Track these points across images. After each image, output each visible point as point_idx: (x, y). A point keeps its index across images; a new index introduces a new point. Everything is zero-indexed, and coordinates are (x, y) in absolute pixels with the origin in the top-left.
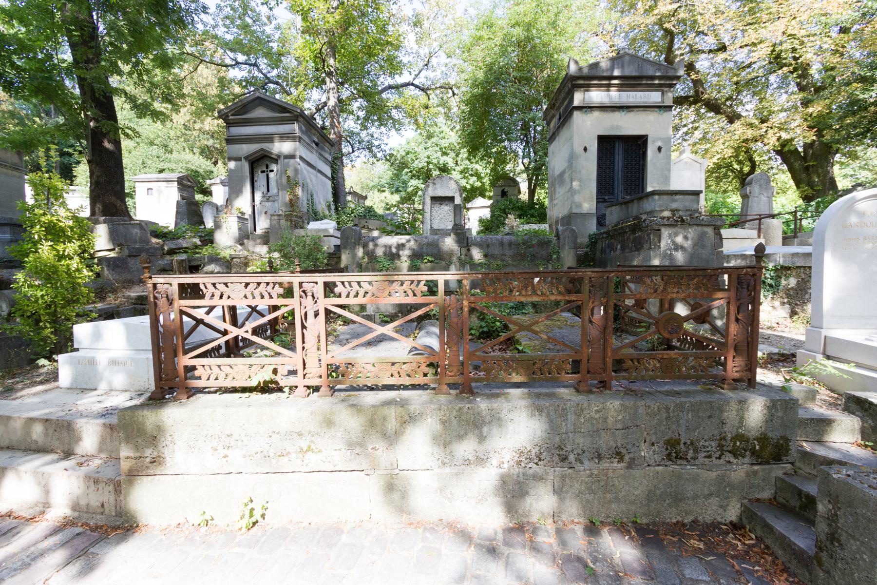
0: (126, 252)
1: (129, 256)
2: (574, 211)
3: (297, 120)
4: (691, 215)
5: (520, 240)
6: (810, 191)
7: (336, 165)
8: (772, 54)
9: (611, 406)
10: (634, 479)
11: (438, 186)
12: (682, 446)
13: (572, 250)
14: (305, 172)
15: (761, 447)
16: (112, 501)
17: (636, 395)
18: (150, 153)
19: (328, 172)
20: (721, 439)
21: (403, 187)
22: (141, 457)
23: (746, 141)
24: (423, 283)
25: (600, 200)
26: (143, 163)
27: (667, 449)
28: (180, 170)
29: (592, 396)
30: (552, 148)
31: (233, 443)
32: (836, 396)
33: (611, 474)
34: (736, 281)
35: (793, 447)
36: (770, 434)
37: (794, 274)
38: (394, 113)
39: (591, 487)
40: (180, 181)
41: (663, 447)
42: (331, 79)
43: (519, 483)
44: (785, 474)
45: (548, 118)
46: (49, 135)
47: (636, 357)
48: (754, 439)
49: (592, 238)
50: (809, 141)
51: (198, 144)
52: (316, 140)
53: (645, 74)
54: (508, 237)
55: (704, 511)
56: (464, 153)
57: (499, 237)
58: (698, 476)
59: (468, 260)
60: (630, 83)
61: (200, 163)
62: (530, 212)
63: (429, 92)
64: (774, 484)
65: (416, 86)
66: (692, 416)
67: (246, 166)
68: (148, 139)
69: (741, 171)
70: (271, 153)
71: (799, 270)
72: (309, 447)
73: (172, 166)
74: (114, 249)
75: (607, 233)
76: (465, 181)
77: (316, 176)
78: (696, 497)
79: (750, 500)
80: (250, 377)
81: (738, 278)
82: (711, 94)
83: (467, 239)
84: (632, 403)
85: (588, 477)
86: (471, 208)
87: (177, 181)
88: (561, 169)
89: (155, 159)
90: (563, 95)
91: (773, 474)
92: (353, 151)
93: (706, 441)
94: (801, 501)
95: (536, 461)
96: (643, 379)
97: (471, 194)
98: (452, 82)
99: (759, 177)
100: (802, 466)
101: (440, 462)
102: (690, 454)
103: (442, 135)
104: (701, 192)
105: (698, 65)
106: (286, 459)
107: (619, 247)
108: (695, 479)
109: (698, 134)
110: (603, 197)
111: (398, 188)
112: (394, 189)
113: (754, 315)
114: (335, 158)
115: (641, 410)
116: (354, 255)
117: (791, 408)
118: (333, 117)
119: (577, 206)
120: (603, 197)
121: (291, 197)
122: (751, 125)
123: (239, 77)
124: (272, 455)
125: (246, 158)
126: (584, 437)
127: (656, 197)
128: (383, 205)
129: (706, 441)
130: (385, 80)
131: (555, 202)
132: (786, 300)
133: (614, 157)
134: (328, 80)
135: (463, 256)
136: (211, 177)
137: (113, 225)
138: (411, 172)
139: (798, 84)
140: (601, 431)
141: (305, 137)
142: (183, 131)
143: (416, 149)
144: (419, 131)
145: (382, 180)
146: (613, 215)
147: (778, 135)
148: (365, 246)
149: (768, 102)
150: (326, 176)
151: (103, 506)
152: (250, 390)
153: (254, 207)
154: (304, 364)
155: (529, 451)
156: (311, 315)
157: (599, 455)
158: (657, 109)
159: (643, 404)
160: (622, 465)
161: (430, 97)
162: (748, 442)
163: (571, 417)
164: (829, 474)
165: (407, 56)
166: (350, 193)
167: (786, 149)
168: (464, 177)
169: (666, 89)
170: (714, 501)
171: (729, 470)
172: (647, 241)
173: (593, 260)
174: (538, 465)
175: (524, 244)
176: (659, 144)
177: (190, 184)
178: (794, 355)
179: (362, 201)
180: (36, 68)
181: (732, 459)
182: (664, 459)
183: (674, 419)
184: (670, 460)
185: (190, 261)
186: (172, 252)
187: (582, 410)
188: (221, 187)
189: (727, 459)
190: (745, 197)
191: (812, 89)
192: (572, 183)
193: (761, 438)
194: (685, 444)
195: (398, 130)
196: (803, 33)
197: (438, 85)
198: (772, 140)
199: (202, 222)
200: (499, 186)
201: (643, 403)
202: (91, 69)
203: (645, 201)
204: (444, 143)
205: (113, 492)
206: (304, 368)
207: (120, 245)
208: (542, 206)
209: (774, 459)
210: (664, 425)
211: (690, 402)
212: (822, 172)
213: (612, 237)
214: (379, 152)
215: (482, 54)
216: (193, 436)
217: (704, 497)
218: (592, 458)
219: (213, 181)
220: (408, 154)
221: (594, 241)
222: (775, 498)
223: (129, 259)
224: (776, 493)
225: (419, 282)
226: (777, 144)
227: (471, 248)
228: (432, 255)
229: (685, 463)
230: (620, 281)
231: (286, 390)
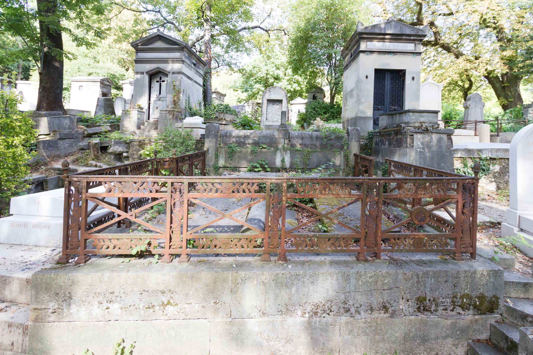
0: (58, 136)
1: (60, 139)
2: (359, 115)
4: (433, 126)
5: (323, 135)
6: (506, 102)
7: (207, 77)
8: (481, 19)
9: (380, 273)
10: (395, 325)
11: (272, 93)
12: (428, 301)
13: (357, 143)
15: (480, 303)
16: (20, 341)
17: (397, 264)
18: (84, 62)
19: (201, 81)
20: (453, 297)
22: (45, 309)
23: (466, 70)
24: (256, 184)
25: (375, 109)
27: (417, 304)
28: (103, 74)
29: (367, 265)
30: (345, 74)
31: (114, 299)
32: (528, 258)
33: (379, 322)
34: (462, 188)
35: (501, 303)
36: (486, 294)
37: (498, 163)
38: (247, 44)
39: (366, 331)
40: (102, 82)
41: (415, 303)
42: (207, 23)
44: (496, 322)
46: (15, 56)
47: (397, 237)
48: (476, 297)
49: (370, 135)
50: (504, 72)
51: (117, 57)
52: (194, 62)
53: (404, 33)
55: (442, 348)
56: (290, 71)
58: (438, 323)
60: (397, 38)
61: (118, 70)
62: (331, 110)
63: (269, 32)
64: (489, 329)
65: (262, 28)
66: (434, 281)
67: (147, 78)
68: (83, 53)
69: (463, 87)
71: (501, 161)
72: (169, 301)
73: (98, 71)
74: (50, 134)
75: (380, 132)
76: (290, 86)
78: (437, 338)
79: (473, 341)
80: (131, 247)
81: (463, 186)
82: (445, 39)
83: (289, 133)
84: (394, 271)
85: (364, 323)
87: (101, 82)
89: (87, 66)
90: (353, 43)
91: (489, 322)
92: (219, 67)
93: (443, 298)
94: (508, 344)
95: (328, 312)
96: (401, 251)
97: (293, 95)
98: (285, 26)
99: (475, 96)
100: (508, 317)
101: (261, 313)
102: (433, 308)
103: (277, 57)
104: (439, 111)
105: (436, 23)
106: (152, 310)
107: (387, 143)
108: (436, 325)
109: (436, 64)
110: (378, 107)
111: (246, 89)
112: (244, 90)
113: (474, 210)
114: (206, 73)
115: (400, 277)
117: (499, 276)
119: (361, 112)
120: (378, 107)
122: (470, 61)
123: (148, 19)
124: (141, 307)
125: (147, 73)
126: (361, 295)
127: (411, 114)
128: (237, 98)
129: (443, 298)
130: (241, 24)
131: (347, 108)
132: (493, 180)
134: (205, 24)
135: (285, 145)
136: (123, 78)
137: (51, 118)
138: (255, 79)
139: (497, 37)
140: (373, 291)
141: (187, 61)
142: (108, 49)
143: (260, 65)
144: (262, 55)
145: (236, 84)
146: (384, 121)
147: (486, 67)
149: (479, 47)
150: (199, 85)
151: (12, 344)
152: (131, 256)
153: (149, 104)
154: (171, 239)
155: (324, 305)
156: (178, 204)
157: (372, 308)
158: (412, 54)
159: (402, 272)
160: (387, 315)
161: (270, 35)
162: (471, 299)
163: (353, 281)
164: (526, 335)
165: (257, 9)
166: (215, 92)
167: (491, 76)
168: (290, 84)
169: (417, 42)
170: (449, 341)
171: (459, 319)
172: (405, 142)
173: (370, 149)
174: (329, 315)
177: (108, 83)
178: (499, 224)
179: (223, 97)
180: (12, 13)
181: (461, 312)
182: (415, 311)
183: (422, 283)
184: (419, 312)
185: (101, 143)
186: (90, 136)
187: (360, 276)
188: (129, 85)
189: (458, 311)
190: (466, 108)
191: (506, 40)
193: (480, 297)
194: (429, 300)
195: (248, 55)
196: (499, 8)
197: (275, 28)
198: (483, 72)
199: (113, 113)
201: (402, 271)
202: (49, 16)
203: (404, 115)
204: (278, 62)
205: (21, 334)
206: (170, 241)
207: (54, 131)
208: (339, 106)
209: (489, 311)
210: (416, 287)
211: (433, 271)
212: (513, 90)
213: (383, 136)
214: (235, 67)
215: (303, 13)
216: (85, 294)
217: (443, 338)
218: (367, 310)
219: (124, 82)
220: (254, 68)
221: (371, 137)
222: (490, 339)
223: (59, 141)
224: (490, 335)
225: (253, 184)
226: (485, 72)
229: (430, 314)
230: (387, 170)
231: (157, 257)
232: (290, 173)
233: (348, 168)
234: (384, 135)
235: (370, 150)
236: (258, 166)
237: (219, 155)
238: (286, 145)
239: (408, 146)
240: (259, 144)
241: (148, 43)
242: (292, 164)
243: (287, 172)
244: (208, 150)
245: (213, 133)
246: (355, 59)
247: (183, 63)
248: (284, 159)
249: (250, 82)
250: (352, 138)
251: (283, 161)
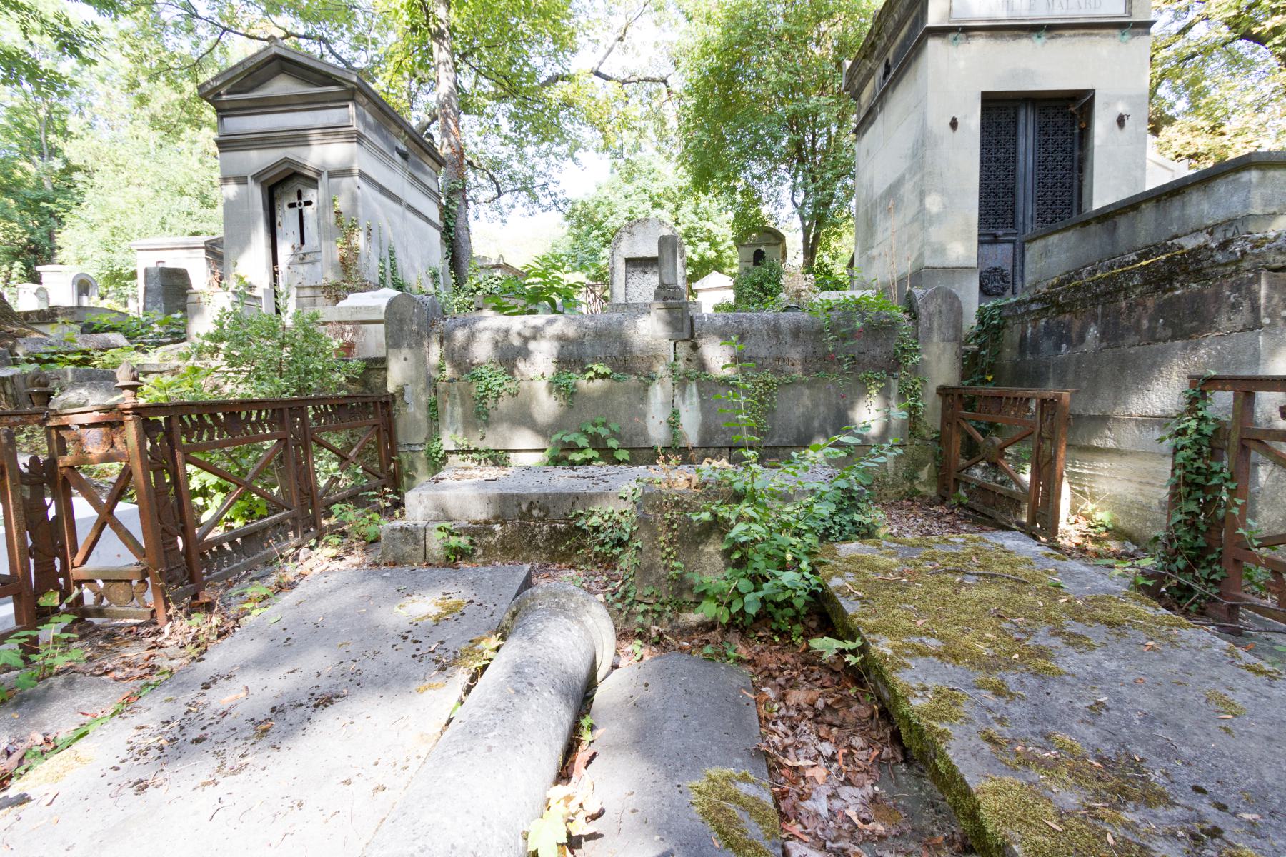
2: (929, 262)
3: (352, 99)
11: (638, 237)
13: (949, 346)
14: (376, 206)
25: (987, 238)
26: (163, 223)
42: (440, 44)
45: (857, 83)
52: (403, 148)
54: (790, 315)
57: (769, 314)
70: (304, 167)
76: (691, 248)
77: (404, 217)
87: (206, 248)
88: (892, 178)
110: (993, 231)
116: (422, 361)
118: (446, 116)
119: (934, 251)
120: (993, 231)
121: (344, 252)
125: (256, 178)
127: (1254, 175)
131: (875, 252)
133: (1015, 143)
134: (435, 46)
138: (603, 235)
143: (611, 198)
148: (445, 338)
150: (427, 220)
153: (275, 273)
158: (1116, 32)
175: (833, 331)
176: (1121, 108)
177: (811, 240)
192: (922, 201)
200: (750, 245)
204: (656, 188)
214: (545, 196)
227: (700, 342)
228: (604, 361)
232: (705, 465)
234: (1071, 303)
235: (990, 373)
236: (583, 442)
239: (1267, 321)
241: (249, 83)
242: (707, 433)
243: (686, 460)
244: (402, 391)
245: (414, 327)
246: (909, 66)
247: (359, 142)
248: (676, 413)
249: (591, 244)
250: (930, 329)
251: (673, 423)
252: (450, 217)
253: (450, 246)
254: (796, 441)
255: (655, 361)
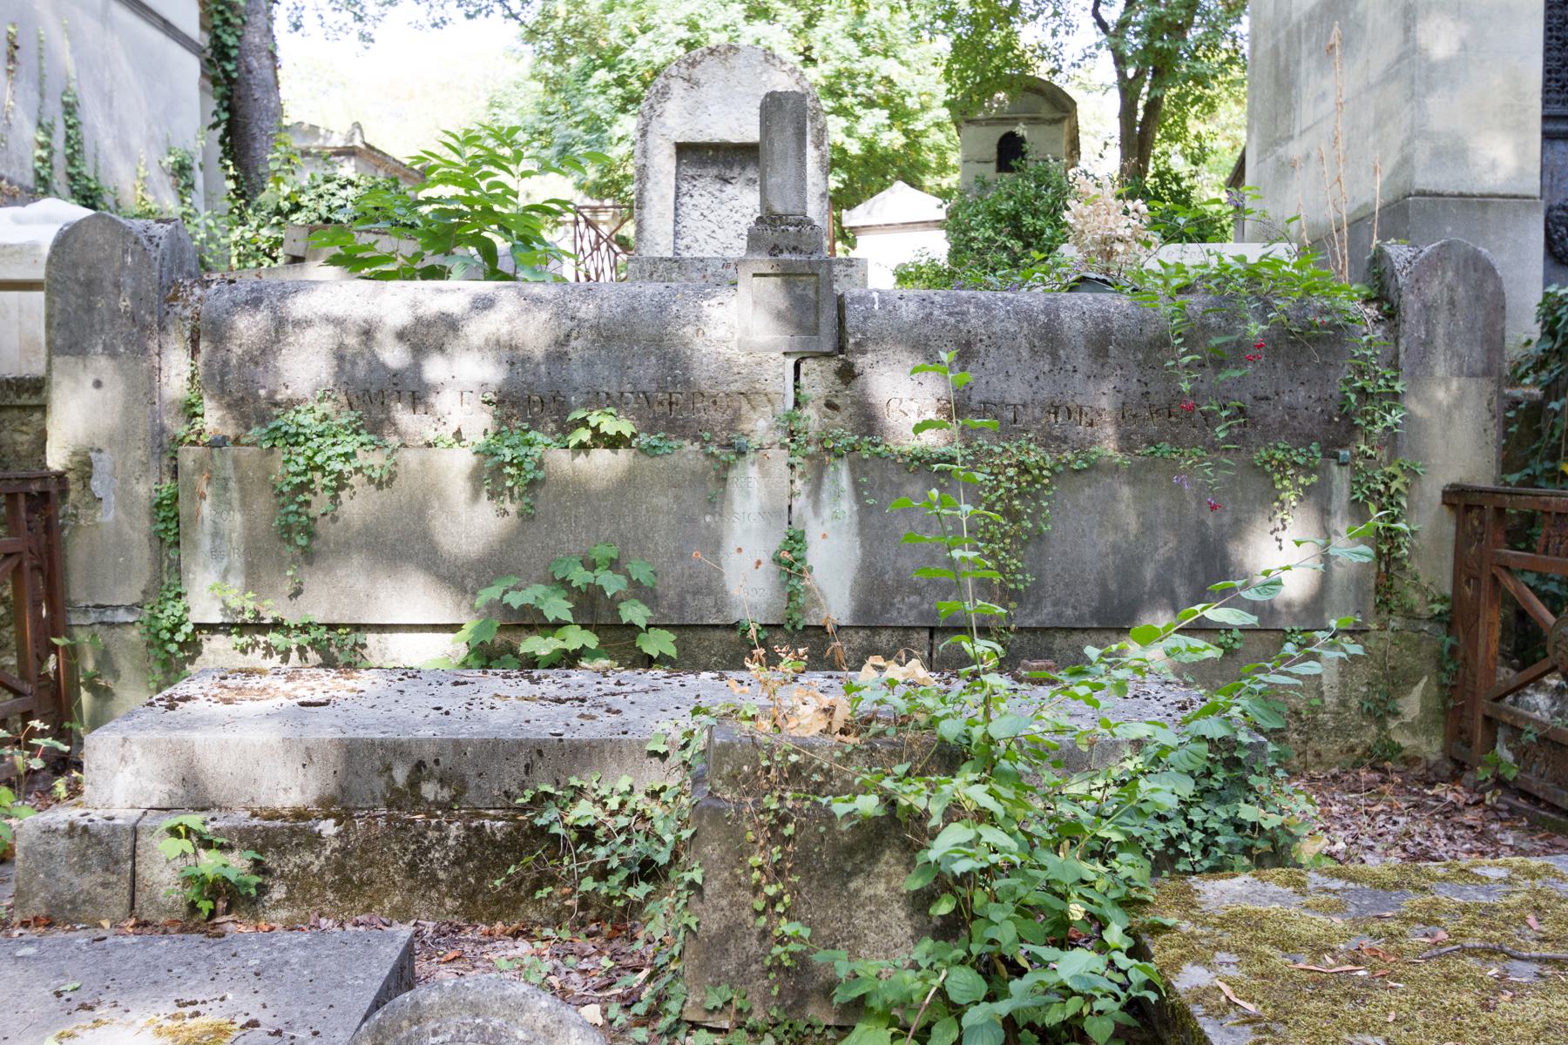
2: (1425, 179)
11: (709, 92)
13: (1472, 386)
21: (589, 144)
43: (766, 10)
54: (1086, 300)
57: (1034, 296)
59: (843, 430)
76: (842, 122)
86: (866, 228)
131: (1295, 150)
145: (503, 115)
150: (167, 27)
166: (349, 152)
175: (1190, 342)
198: (284, 666)
232: (867, 675)
233: (1396, 622)
236: (557, 607)
237: (183, 508)
238: (812, 416)
240: (563, 408)
243: (821, 661)
244: (84, 466)
245: (125, 303)
248: (796, 540)
250: (1427, 344)
252: (226, 22)
253: (224, 97)
254: (1096, 614)
255: (745, 407)
